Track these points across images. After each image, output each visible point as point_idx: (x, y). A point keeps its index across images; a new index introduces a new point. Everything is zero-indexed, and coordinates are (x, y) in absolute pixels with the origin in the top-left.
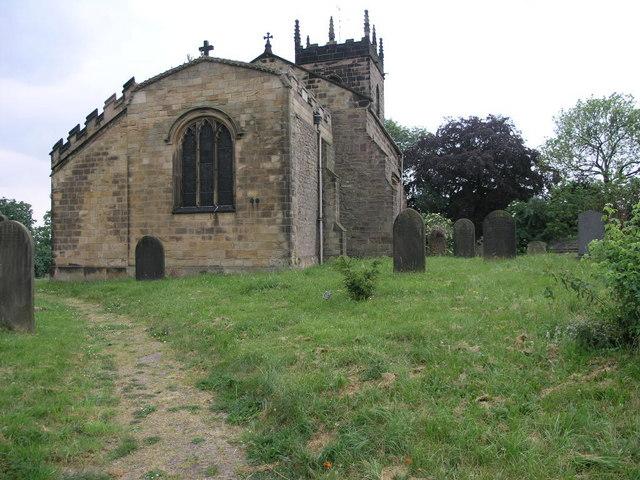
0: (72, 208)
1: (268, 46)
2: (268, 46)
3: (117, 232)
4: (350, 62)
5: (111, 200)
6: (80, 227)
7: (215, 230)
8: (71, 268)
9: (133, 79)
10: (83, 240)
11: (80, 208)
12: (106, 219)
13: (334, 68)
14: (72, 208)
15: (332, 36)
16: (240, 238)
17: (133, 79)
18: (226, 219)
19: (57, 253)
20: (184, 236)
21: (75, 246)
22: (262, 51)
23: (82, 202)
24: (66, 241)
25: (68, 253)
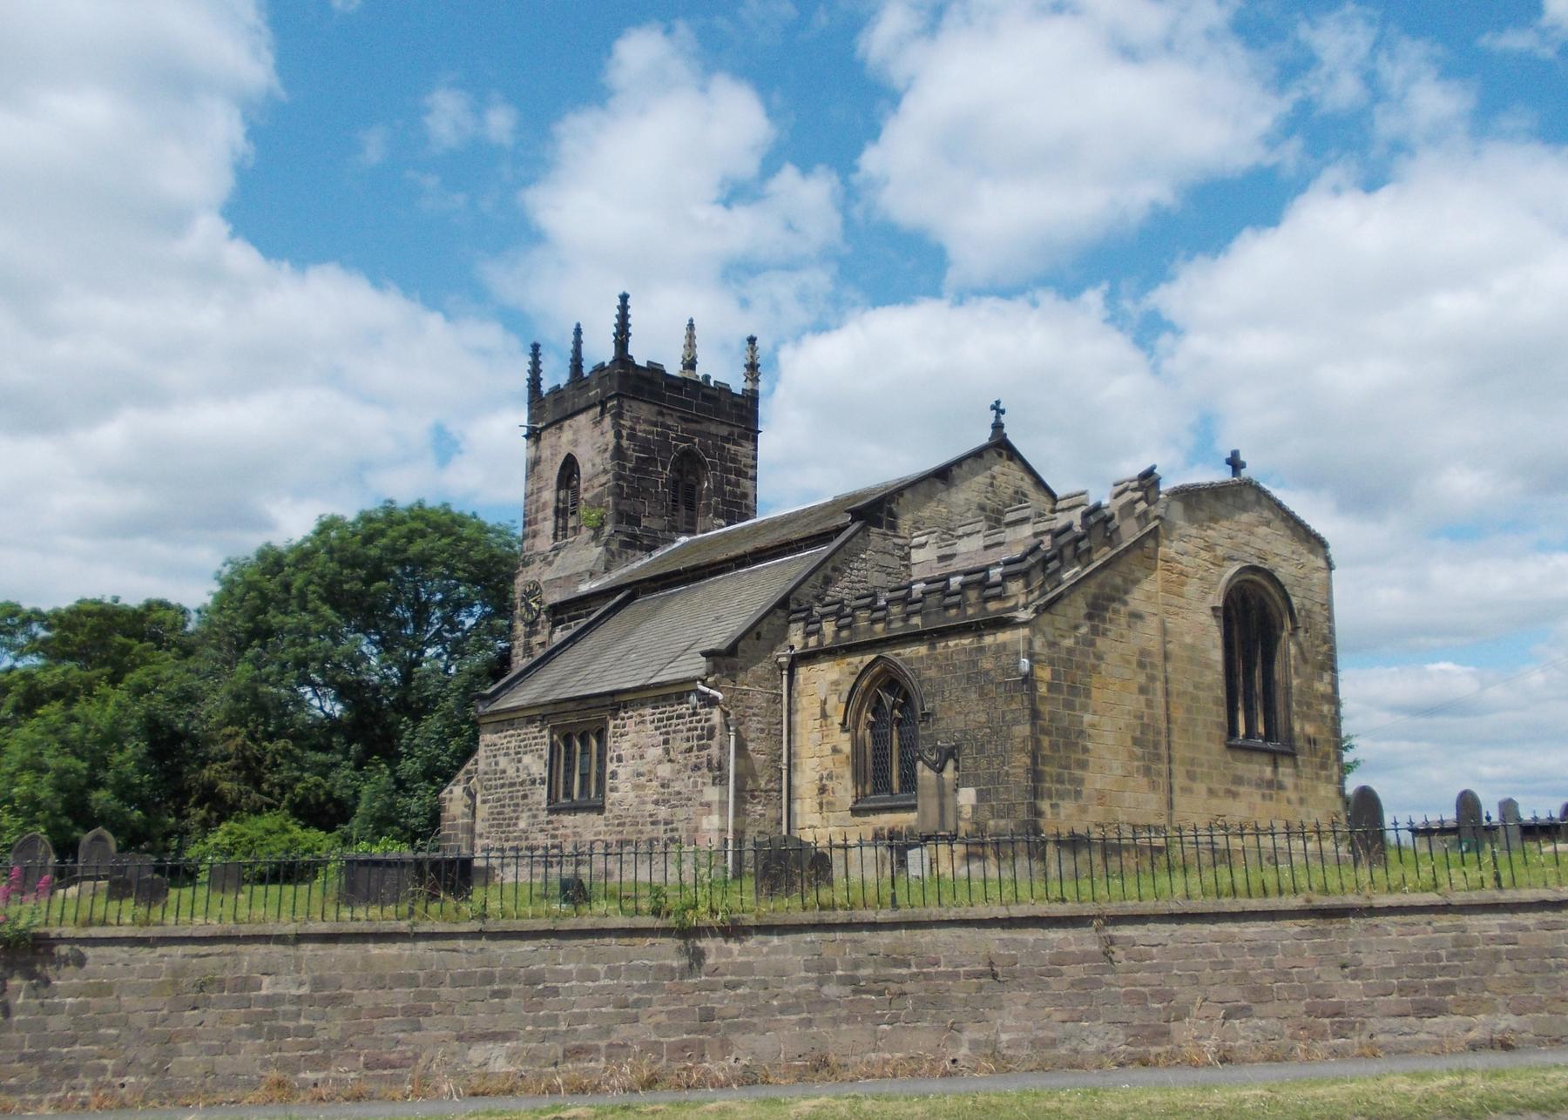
0: (1069, 705)
1: (998, 427)
2: (998, 427)
3: (1147, 771)
4: (724, 431)
5: (1135, 702)
6: (1086, 750)
7: (1274, 785)
8: (1074, 843)
9: (1154, 467)
10: (1094, 781)
11: (1085, 708)
12: (1129, 742)
13: (695, 433)
14: (1069, 705)
15: (690, 364)
16: (1302, 801)
17: (1154, 467)
18: (1285, 772)
19: (1045, 805)
20: (1242, 789)
21: (1078, 794)
22: (983, 437)
23: (1088, 695)
24: (1060, 780)
25: (1067, 807)
